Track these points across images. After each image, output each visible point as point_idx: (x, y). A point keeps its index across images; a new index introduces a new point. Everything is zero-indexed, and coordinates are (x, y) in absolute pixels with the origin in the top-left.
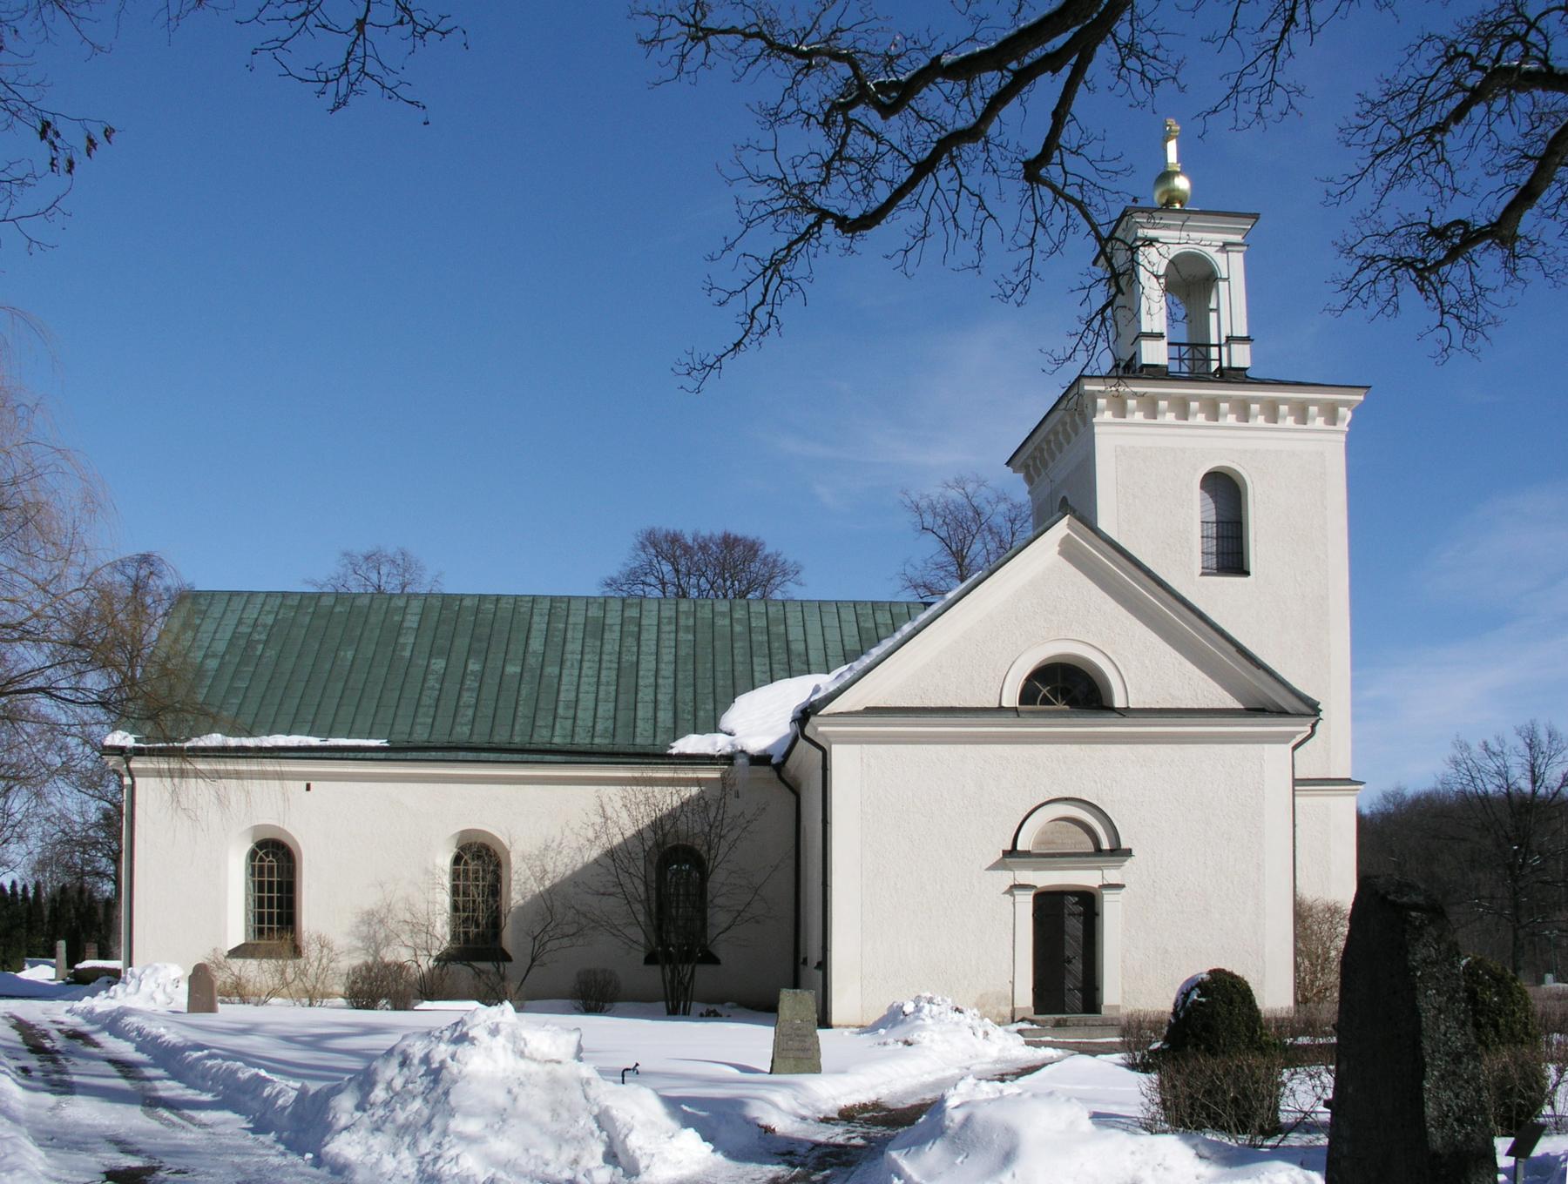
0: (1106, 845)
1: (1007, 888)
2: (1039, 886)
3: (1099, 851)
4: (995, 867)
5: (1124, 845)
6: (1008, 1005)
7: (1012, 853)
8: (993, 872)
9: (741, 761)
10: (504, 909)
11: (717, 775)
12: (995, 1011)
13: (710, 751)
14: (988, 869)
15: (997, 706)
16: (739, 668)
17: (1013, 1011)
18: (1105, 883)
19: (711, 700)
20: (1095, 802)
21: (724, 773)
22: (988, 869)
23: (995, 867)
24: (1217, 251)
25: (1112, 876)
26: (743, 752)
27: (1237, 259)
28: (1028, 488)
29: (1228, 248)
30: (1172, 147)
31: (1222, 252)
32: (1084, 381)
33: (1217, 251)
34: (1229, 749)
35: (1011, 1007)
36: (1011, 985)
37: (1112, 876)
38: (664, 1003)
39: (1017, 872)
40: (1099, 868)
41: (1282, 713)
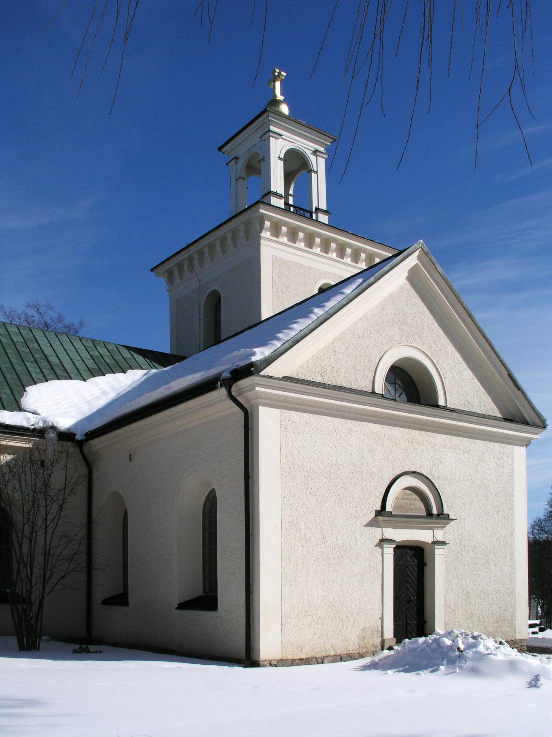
0: (435, 512)
1: (377, 541)
2: (397, 541)
3: (430, 514)
4: (370, 524)
5: (446, 512)
6: (378, 637)
7: (382, 512)
8: (368, 528)
9: (52, 435)
10: (435, 545)
11: (29, 446)
12: (371, 643)
13: (25, 424)
14: (366, 526)
15: (371, 391)
16: (18, 368)
17: (383, 641)
18: (435, 540)
19: (6, 387)
20: (429, 477)
21: (35, 444)
22: (366, 526)
23: (370, 524)
24: (311, 154)
25: (439, 535)
26: (53, 428)
27: (322, 162)
28: (167, 287)
29: (318, 154)
30: (278, 85)
31: (314, 155)
32: (261, 205)
33: (311, 154)
34: (480, 445)
35: (380, 639)
36: (380, 621)
37: (439, 535)
38: (15, 639)
39: (384, 529)
40: (431, 529)
41: (525, 423)
